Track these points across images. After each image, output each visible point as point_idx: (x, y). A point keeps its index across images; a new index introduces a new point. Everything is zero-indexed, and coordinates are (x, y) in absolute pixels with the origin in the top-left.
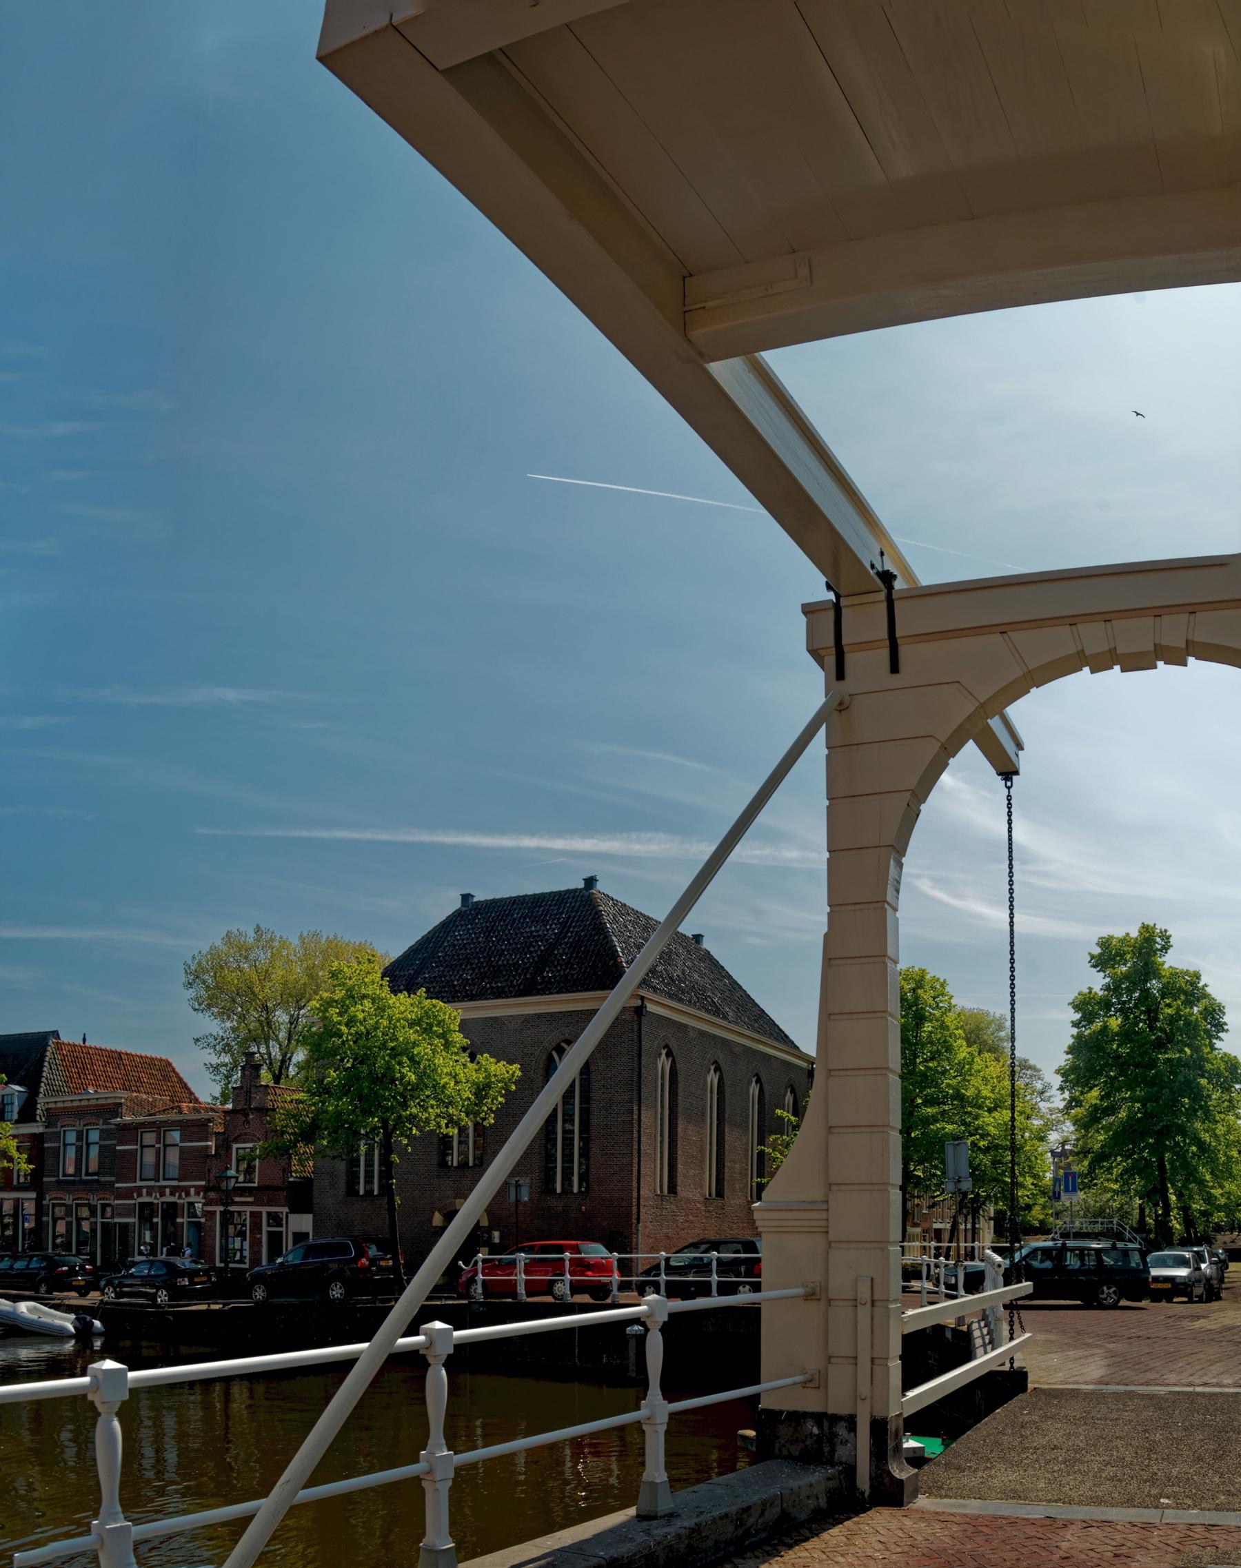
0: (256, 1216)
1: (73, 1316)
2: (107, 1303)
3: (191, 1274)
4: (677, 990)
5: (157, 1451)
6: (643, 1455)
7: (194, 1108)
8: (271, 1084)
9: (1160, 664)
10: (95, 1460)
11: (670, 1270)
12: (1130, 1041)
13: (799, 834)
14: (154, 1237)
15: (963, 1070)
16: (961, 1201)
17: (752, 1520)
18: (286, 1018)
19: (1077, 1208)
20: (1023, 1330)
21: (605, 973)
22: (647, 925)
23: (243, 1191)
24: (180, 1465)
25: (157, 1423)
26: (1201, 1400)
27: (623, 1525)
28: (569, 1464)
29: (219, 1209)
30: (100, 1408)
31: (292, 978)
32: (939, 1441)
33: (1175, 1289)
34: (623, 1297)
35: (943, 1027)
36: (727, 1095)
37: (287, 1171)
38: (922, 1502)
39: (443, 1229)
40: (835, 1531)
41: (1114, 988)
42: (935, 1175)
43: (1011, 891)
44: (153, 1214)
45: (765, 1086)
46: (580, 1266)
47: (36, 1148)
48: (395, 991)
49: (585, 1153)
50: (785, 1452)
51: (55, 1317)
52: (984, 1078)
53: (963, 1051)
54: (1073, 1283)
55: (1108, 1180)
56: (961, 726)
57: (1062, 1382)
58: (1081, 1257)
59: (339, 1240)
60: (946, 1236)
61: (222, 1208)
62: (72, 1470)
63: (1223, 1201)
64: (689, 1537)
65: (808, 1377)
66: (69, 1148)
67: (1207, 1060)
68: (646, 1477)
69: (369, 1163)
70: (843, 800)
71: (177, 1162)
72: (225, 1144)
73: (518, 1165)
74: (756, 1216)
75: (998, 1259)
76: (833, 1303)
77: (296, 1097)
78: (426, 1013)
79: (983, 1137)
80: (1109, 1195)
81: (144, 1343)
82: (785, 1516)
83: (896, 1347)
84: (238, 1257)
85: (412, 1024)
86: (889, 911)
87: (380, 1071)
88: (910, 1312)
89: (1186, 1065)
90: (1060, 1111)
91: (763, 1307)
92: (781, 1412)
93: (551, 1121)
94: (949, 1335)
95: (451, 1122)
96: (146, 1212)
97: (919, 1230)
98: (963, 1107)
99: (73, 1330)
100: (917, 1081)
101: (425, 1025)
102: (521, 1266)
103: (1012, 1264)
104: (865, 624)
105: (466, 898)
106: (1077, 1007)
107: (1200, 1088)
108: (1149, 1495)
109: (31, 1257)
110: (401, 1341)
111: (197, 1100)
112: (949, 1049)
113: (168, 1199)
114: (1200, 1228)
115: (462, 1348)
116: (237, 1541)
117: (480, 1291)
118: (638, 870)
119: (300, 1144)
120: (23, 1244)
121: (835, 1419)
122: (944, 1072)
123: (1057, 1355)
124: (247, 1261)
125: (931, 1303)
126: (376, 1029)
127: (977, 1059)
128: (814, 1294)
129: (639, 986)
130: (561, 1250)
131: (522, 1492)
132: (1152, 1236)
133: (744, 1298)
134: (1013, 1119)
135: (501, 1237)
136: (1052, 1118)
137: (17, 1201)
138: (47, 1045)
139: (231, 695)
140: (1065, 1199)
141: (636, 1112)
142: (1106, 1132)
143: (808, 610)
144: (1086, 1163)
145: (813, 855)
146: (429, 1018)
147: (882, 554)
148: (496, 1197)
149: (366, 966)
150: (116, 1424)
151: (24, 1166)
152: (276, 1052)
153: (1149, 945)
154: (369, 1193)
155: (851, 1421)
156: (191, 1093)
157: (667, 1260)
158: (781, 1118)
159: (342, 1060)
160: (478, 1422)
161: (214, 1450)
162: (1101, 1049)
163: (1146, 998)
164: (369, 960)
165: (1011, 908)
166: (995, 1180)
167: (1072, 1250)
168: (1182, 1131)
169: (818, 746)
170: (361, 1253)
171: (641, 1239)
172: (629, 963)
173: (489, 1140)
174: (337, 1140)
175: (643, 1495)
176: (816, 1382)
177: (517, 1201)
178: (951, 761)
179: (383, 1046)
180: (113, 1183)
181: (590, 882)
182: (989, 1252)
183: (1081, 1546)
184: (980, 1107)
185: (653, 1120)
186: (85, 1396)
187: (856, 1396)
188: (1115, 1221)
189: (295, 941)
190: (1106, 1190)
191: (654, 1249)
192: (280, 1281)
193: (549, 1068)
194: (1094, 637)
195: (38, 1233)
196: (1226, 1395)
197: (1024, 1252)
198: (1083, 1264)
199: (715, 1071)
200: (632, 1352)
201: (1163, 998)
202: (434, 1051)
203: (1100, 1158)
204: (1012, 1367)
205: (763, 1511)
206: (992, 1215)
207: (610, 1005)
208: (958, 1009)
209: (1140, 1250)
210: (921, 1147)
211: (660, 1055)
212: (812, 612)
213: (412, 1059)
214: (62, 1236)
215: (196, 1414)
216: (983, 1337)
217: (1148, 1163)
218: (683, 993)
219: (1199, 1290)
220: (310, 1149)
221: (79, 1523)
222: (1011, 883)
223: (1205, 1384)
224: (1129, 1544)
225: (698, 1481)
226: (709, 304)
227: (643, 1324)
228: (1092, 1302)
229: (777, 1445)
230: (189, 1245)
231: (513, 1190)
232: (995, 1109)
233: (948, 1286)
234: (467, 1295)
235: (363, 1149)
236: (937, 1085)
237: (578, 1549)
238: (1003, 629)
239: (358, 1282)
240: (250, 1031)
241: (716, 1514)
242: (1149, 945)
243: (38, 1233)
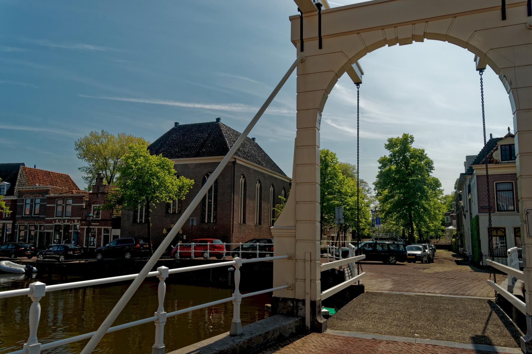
0: (99, 230)
1: (25, 266)
2: (39, 261)
3: (74, 250)
4: (247, 156)
5: (55, 315)
6: (232, 313)
7: (78, 192)
8: (107, 184)
9: (414, 42)
10: (28, 320)
11: (243, 249)
12: (399, 173)
13: (287, 105)
14: (60, 237)
15: (341, 183)
16: (341, 227)
17: (270, 336)
18: (113, 162)
20: (362, 271)
21: (223, 150)
22: (237, 134)
24: (63, 320)
25: (56, 304)
26: (427, 298)
27: (225, 338)
28: (207, 316)
29: (86, 227)
30: (33, 299)
31: (115, 148)
32: (334, 309)
33: (416, 259)
34: (227, 258)
35: (334, 169)
36: (263, 191)
37: (112, 214)
38: (329, 331)
39: (167, 234)
40: (298, 341)
41: (393, 156)
43: (358, 123)
44: (60, 229)
46: (213, 247)
47: (13, 205)
48: (152, 154)
49: (215, 209)
50: (281, 312)
51: (17, 266)
52: (348, 186)
53: (341, 177)
54: (380, 255)
56: (342, 67)
57: (376, 290)
58: (382, 246)
59: (129, 238)
60: (335, 238)
62: (18, 324)
63: (433, 228)
64: (248, 343)
65: (289, 286)
66: (37, 205)
67: (427, 180)
68: (233, 321)
69: (141, 212)
70: (302, 93)
71: (70, 211)
72: (89, 205)
73: (193, 213)
74: (272, 231)
75: (353, 246)
77: (116, 189)
79: (348, 205)
81: (53, 275)
82: (281, 335)
83: (319, 276)
84: (92, 244)
86: (317, 130)
87: (146, 181)
88: (323, 264)
89: (419, 181)
90: (374, 197)
91: (274, 262)
92: (280, 298)
93: (204, 199)
94: (337, 272)
95: (170, 198)
96: (57, 228)
97: (326, 236)
99: (24, 271)
100: (325, 187)
101: (162, 166)
102: (193, 247)
103: (358, 248)
104: (310, 31)
105: (176, 124)
106: (380, 162)
107: (424, 189)
108: (410, 332)
109: (9, 244)
110: (150, 273)
111: (79, 189)
112: (336, 176)
113: (66, 223)
114: (425, 237)
115: (171, 275)
116: (83, 348)
117: (178, 255)
118: (234, 116)
119: (117, 205)
120: (6, 240)
121: (298, 301)
122: (335, 184)
123: (375, 280)
125: (330, 261)
126: (145, 167)
127: (346, 180)
129: (234, 154)
130: (206, 242)
131: (190, 326)
132: (407, 240)
133: (267, 258)
134: (358, 200)
135: (186, 237)
136: (372, 199)
137: (4, 224)
138: (20, 168)
139: (91, 47)
140: (376, 227)
143: (292, 19)
144: (383, 214)
145: (292, 112)
148: (185, 224)
149: (141, 146)
150: (39, 306)
151: (8, 211)
152: (109, 174)
153: (406, 140)
154: (141, 222)
155: (303, 302)
156: (77, 187)
157: (242, 245)
158: (280, 199)
159: (133, 177)
160: (176, 301)
161: (76, 315)
162: (389, 176)
163: (405, 159)
165: (358, 129)
167: (379, 244)
168: (418, 204)
170: (137, 242)
171: (234, 238)
172: (231, 147)
173: (183, 205)
174: (130, 204)
175: (232, 327)
177: (192, 225)
178: (339, 79)
179: (147, 173)
180: (45, 218)
181: (218, 120)
182: (350, 244)
183: (386, 350)
184: (347, 196)
185: (238, 199)
186: (27, 296)
187: (305, 293)
188: (394, 234)
189: (116, 136)
190: (391, 224)
191: (238, 242)
192: (107, 252)
193: (204, 181)
194: (390, 33)
195: (12, 237)
196: (437, 297)
197: (362, 244)
198: (383, 249)
200: (230, 277)
202: (165, 175)
203: (388, 213)
205: (273, 333)
207: (224, 161)
208: (340, 163)
209: (403, 245)
210: (327, 209)
213: (157, 177)
214: (22, 237)
215: (71, 301)
216: (348, 273)
217: (406, 215)
219: (425, 259)
220: (120, 207)
221: (18, 345)
222: (358, 120)
223: (429, 293)
224: (404, 351)
225: (251, 322)
227: (234, 267)
228: (386, 262)
229: (278, 310)
230: (74, 240)
231: (191, 221)
232: (352, 196)
233: (336, 256)
234: (174, 257)
235: (139, 207)
236: (332, 188)
237: (209, 347)
238: (358, 32)
239: (135, 253)
241: (257, 334)
242: (406, 140)
243: (12, 237)
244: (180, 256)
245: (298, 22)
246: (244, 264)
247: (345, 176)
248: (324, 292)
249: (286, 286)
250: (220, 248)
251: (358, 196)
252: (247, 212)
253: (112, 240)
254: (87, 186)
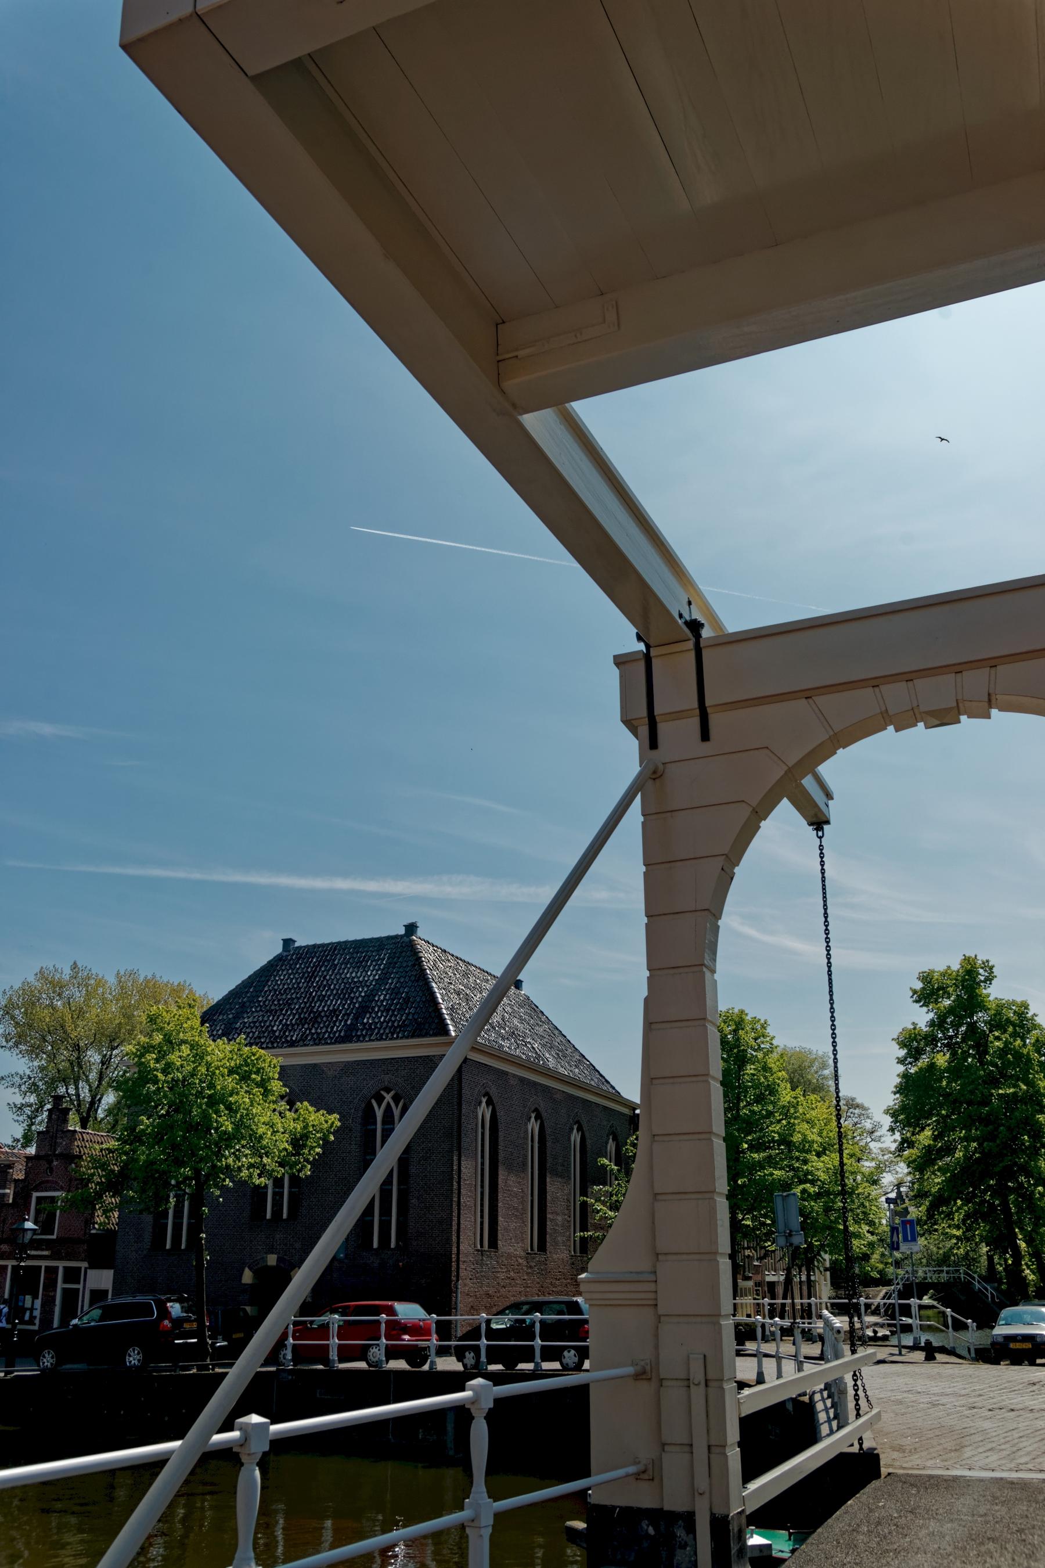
19: (920, 1256)
23: (36, 1244)
32: (784, 1533)
35: (766, 1068)
36: (549, 1144)
37: (89, 1221)
41: (939, 1023)
42: (764, 1224)
45: (587, 1135)
46: (397, 1328)
53: (786, 1095)
55: (949, 1227)
59: (140, 1299)
60: (780, 1290)
61: (15, 1263)
65: (641, 1467)
76: (665, 1383)
78: (245, 1060)
80: (954, 1241)
83: (733, 1434)
84: (27, 1317)
85: (231, 1072)
86: (708, 974)
92: (614, 1508)
93: (369, 1210)
97: (750, 1284)
98: (790, 1151)
100: (740, 1125)
101: (243, 1073)
102: (334, 1329)
104: (675, 694)
105: (287, 943)
106: (902, 1044)
117: (289, 1357)
124: (37, 1321)
128: (644, 1372)
130: (376, 1311)
136: (885, 1163)
139: (47, 729)
141: (455, 1163)
142: (944, 1174)
143: (620, 661)
144: (923, 1208)
146: (247, 1065)
147: (690, 603)
149: (186, 1011)
152: (85, 1093)
153: (970, 979)
155: (688, 1519)
157: (488, 1322)
159: (156, 1107)
164: (190, 1005)
166: (830, 1228)
169: (635, 814)
171: (462, 1300)
176: (649, 1474)
181: (411, 928)
184: (808, 1151)
185: (470, 1170)
187: (694, 1492)
188: (962, 1269)
191: (474, 1310)
199: (536, 1119)
201: (991, 1031)
204: (861, 1448)
206: (828, 1265)
210: (748, 1195)
211: (480, 1103)
212: (624, 663)
213: (229, 1107)
216: (826, 1410)
218: (503, 1039)
226: (521, 353)
240: (59, 1071)
242: (970, 979)
244: (296, 1360)
245: (640, 674)
246: (497, 1401)
247: (799, 1091)
248: (753, 1486)
249: (632, 1469)
250: (417, 1330)
251: (841, 1152)
252: (501, 1211)
253: (86, 1308)
254: (19, 1132)
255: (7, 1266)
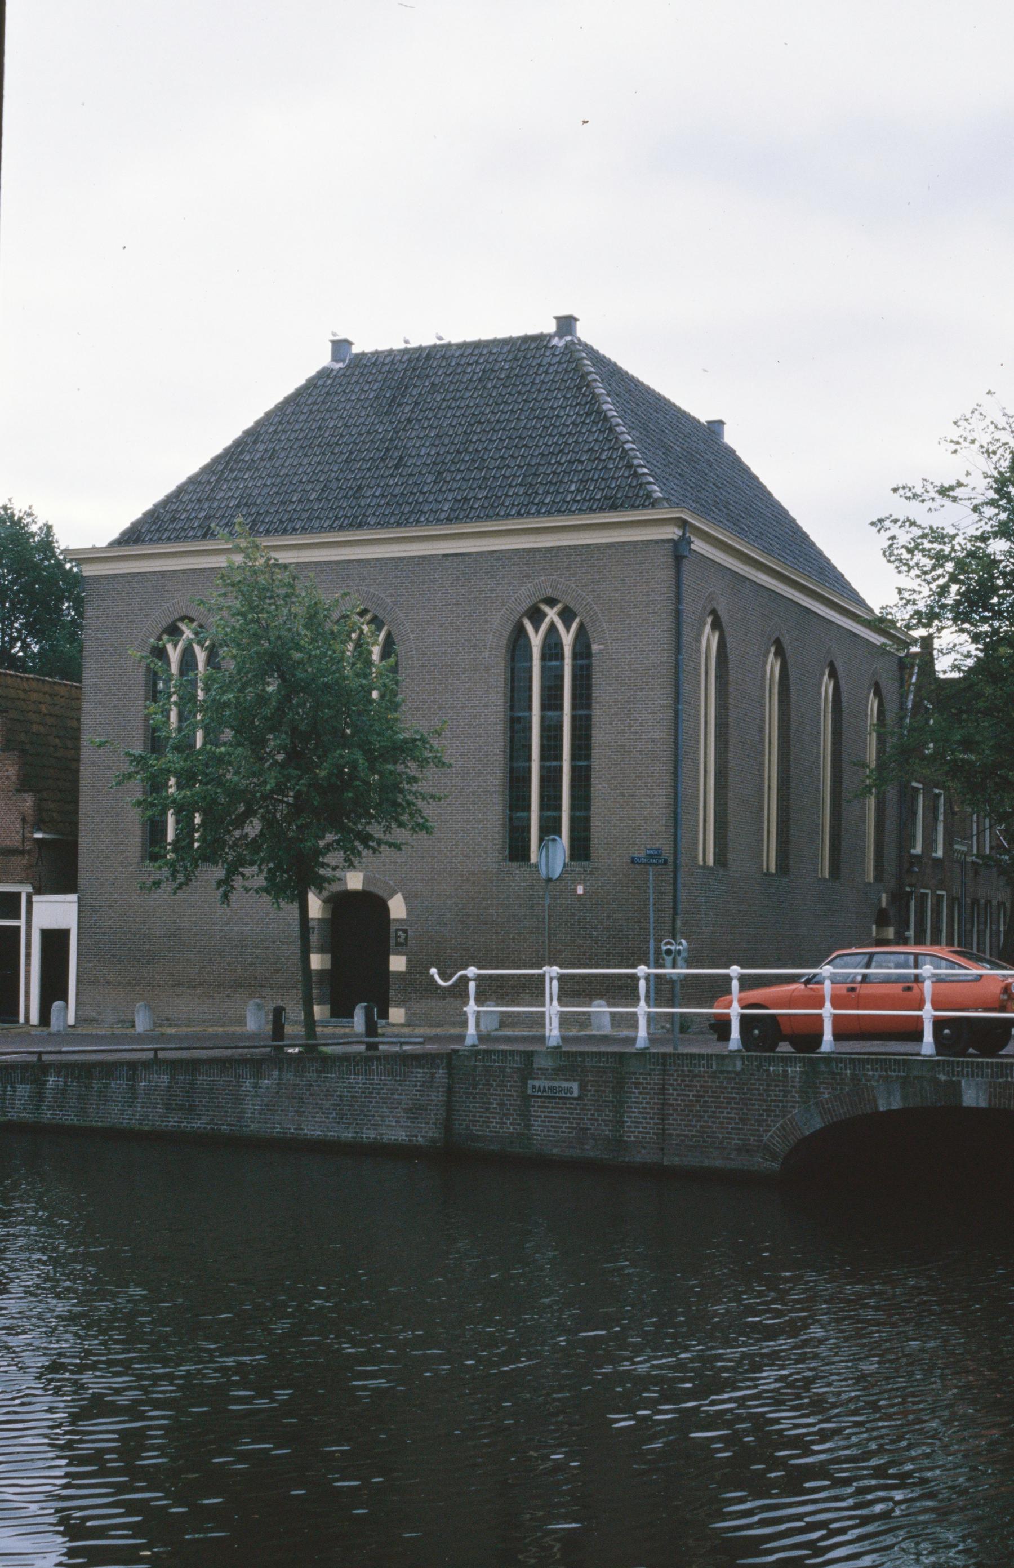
45: (842, 682)
255: (19, 894)
